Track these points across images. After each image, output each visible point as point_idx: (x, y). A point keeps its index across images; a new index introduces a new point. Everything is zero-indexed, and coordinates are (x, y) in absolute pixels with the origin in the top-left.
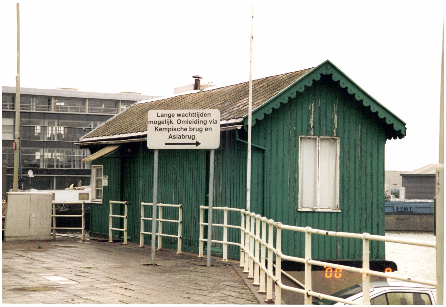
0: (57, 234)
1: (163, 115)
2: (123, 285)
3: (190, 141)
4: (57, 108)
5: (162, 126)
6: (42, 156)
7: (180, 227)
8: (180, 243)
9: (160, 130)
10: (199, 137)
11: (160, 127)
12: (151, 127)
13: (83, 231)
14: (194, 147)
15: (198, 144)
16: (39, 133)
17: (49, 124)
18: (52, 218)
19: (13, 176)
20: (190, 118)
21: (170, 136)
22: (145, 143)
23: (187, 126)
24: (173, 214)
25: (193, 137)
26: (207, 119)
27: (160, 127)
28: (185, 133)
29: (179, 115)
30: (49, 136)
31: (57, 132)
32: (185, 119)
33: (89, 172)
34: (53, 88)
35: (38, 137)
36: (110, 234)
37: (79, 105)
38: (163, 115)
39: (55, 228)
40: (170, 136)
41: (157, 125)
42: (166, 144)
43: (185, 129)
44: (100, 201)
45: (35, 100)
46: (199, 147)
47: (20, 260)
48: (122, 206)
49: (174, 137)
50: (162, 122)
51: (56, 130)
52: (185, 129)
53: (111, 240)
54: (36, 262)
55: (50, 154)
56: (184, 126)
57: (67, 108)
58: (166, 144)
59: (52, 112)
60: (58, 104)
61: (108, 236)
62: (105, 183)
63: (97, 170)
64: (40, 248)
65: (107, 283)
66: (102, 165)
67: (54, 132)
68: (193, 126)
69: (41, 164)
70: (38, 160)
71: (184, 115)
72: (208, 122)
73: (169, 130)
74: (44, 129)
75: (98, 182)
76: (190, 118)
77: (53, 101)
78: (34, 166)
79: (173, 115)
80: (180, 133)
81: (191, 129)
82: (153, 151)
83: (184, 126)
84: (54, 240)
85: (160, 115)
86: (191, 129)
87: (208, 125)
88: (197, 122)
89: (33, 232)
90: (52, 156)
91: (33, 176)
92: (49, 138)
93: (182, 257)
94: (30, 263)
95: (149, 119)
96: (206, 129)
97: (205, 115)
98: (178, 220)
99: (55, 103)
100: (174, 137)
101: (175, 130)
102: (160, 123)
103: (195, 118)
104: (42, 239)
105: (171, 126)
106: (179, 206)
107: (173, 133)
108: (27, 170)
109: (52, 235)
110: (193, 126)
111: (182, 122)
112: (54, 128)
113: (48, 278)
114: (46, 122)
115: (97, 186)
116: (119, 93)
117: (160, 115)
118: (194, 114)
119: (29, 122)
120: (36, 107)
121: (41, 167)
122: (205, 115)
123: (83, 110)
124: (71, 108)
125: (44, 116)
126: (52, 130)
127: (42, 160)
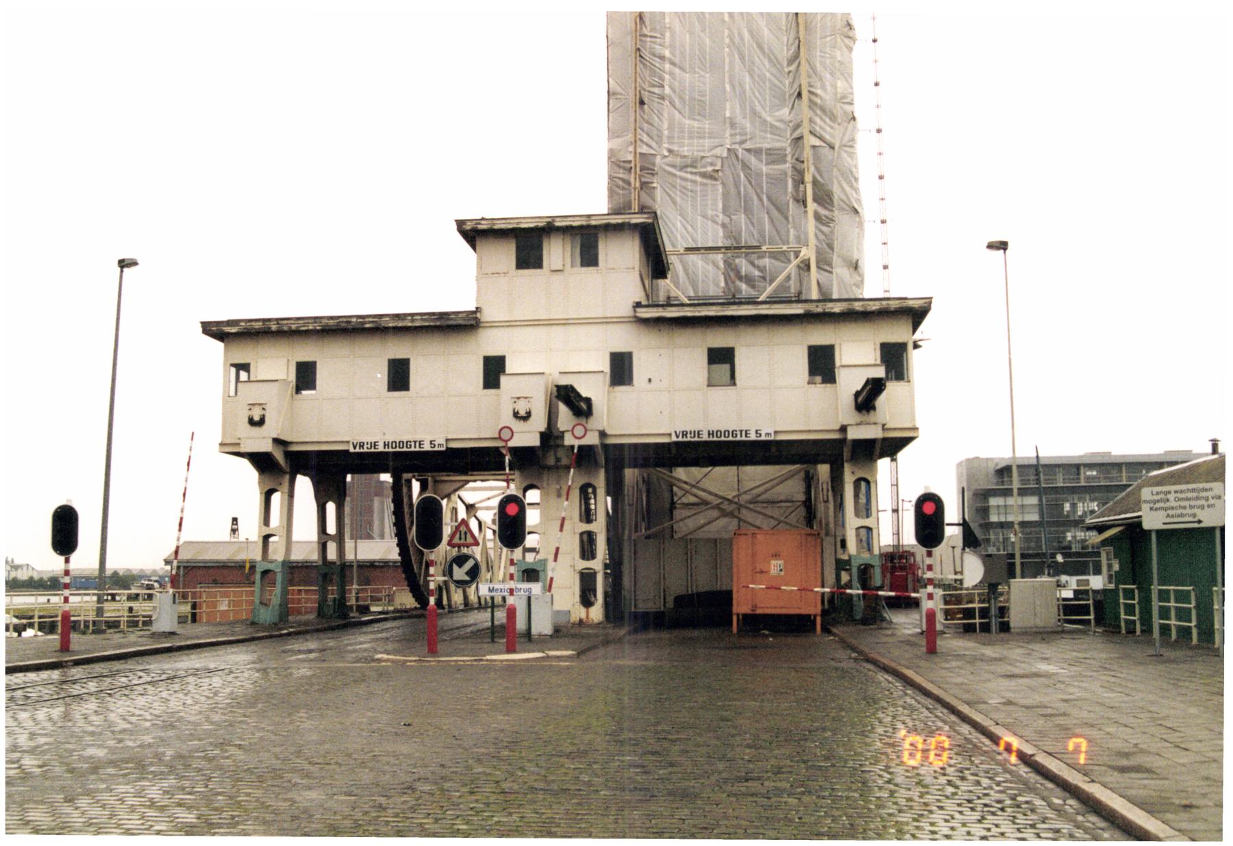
0: (1065, 625)
1: (1158, 493)
2: (1113, 673)
3: (1191, 519)
4: (1088, 478)
5: (1158, 505)
6: (1074, 537)
7: (1194, 613)
8: (1195, 632)
9: (1156, 509)
10: (1201, 515)
11: (1155, 506)
12: (1145, 507)
13: (1093, 622)
14: (1196, 525)
15: (1200, 522)
16: (1068, 512)
17: (1080, 499)
18: (1058, 605)
19: (1100, 561)
20: (1190, 495)
21: (1168, 516)
22: (1139, 524)
23: (1187, 503)
24: (1182, 597)
25: (1194, 515)
26: (1209, 494)
27: (1155, 506)
28: (1185, 512)
29: (1176, 492)
30: (1080, 513)
31: (1090, 509)
32: (1183, 496)
33: (1098, 555)
34: (1082, 453)
35: (1068, 516)
36: (1123, 624)
37: (1114, 473)
38: (1158, 493)
39: (1062, 617)
40: (1168, 516)
41: (1152, 505)
42: (1164, 524)
43: (1184, 508)
44: (1112, 586)
45: (1061, 469)
46: (1202, 525)
47: (1019, 651)
48: (1133, 590)
49: (1173, 516)
50: (1158, 501)
51: (1088, 507)
52: (1184, 508)
53: (1124, 632)
54: (1035, 653)
55: (1083, 534)
56: (1183, 503)
57: (1099, 478)
58: (1164, 524)
59: (1083, 484)
60: (1089, 473)
61: (1119, 627)
62: (1116, 567)
63: (1108, 554)
64: (1043, 639)
65: (1098, 671)
66: (1112, 548)
67: (1086, 509)
68: (1193, 503)
69: (1073, 546)
70: (1070, 541)
71: (1182, 492)
72: (1210, 498)
73: (1166, 509)
74: (1074, 506)
75: (1110, 567)
76: (1190, 495)
77: (1082, 468)
78: (1064, 548)
79: (1170, 492)
80: (1179, 512)
81: (1191, 507)
82: (1150, 531)
83: (1183, 503)
84: (1063, 632)
85: (1154, 493)
86: (1191, 507)
87: (1211, 502)
88: (1197, 498)
89: (1040, 623)
90: (1085, 536)
91: (1062, 561)
92: (1080, 516)
93: (1197, 647)
94: (1028, 654)
95: (1143, 498)
96: (1209, 506)
97: (1206, 490)
98: (1190, 604)
99: (1085, 473)
100: (1173, 516)
101: (1173, 508)
102: (1156, 502)
103: (1195, 495)
104: (1049, 630)
105: (1168, 504)
106: (1191, 588)
107: (1171, 512)
108: (1056, 554)
109: (1059, 626)
110: (1193, 503)
111: (1179, 500)
112: (1086, 505)
113: (1039, 667)
114: (1076, 496)
115: (1109, 571)
116: (1162, 452)
117: (1154, 493)
118: (1193, 490)
119: (1056, 500)
120: (1064, 479)
121: (1074, 550)
122: (1206, 490)
123: (1119, 479)
124: (1105, 478)
125: (1073, 490)
126: (1084, 507)
127: (1074, 541)
